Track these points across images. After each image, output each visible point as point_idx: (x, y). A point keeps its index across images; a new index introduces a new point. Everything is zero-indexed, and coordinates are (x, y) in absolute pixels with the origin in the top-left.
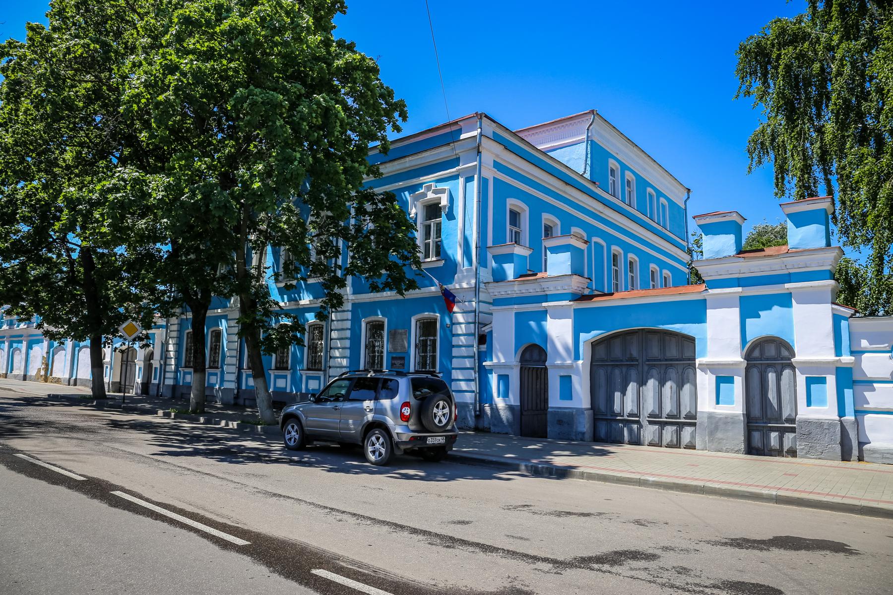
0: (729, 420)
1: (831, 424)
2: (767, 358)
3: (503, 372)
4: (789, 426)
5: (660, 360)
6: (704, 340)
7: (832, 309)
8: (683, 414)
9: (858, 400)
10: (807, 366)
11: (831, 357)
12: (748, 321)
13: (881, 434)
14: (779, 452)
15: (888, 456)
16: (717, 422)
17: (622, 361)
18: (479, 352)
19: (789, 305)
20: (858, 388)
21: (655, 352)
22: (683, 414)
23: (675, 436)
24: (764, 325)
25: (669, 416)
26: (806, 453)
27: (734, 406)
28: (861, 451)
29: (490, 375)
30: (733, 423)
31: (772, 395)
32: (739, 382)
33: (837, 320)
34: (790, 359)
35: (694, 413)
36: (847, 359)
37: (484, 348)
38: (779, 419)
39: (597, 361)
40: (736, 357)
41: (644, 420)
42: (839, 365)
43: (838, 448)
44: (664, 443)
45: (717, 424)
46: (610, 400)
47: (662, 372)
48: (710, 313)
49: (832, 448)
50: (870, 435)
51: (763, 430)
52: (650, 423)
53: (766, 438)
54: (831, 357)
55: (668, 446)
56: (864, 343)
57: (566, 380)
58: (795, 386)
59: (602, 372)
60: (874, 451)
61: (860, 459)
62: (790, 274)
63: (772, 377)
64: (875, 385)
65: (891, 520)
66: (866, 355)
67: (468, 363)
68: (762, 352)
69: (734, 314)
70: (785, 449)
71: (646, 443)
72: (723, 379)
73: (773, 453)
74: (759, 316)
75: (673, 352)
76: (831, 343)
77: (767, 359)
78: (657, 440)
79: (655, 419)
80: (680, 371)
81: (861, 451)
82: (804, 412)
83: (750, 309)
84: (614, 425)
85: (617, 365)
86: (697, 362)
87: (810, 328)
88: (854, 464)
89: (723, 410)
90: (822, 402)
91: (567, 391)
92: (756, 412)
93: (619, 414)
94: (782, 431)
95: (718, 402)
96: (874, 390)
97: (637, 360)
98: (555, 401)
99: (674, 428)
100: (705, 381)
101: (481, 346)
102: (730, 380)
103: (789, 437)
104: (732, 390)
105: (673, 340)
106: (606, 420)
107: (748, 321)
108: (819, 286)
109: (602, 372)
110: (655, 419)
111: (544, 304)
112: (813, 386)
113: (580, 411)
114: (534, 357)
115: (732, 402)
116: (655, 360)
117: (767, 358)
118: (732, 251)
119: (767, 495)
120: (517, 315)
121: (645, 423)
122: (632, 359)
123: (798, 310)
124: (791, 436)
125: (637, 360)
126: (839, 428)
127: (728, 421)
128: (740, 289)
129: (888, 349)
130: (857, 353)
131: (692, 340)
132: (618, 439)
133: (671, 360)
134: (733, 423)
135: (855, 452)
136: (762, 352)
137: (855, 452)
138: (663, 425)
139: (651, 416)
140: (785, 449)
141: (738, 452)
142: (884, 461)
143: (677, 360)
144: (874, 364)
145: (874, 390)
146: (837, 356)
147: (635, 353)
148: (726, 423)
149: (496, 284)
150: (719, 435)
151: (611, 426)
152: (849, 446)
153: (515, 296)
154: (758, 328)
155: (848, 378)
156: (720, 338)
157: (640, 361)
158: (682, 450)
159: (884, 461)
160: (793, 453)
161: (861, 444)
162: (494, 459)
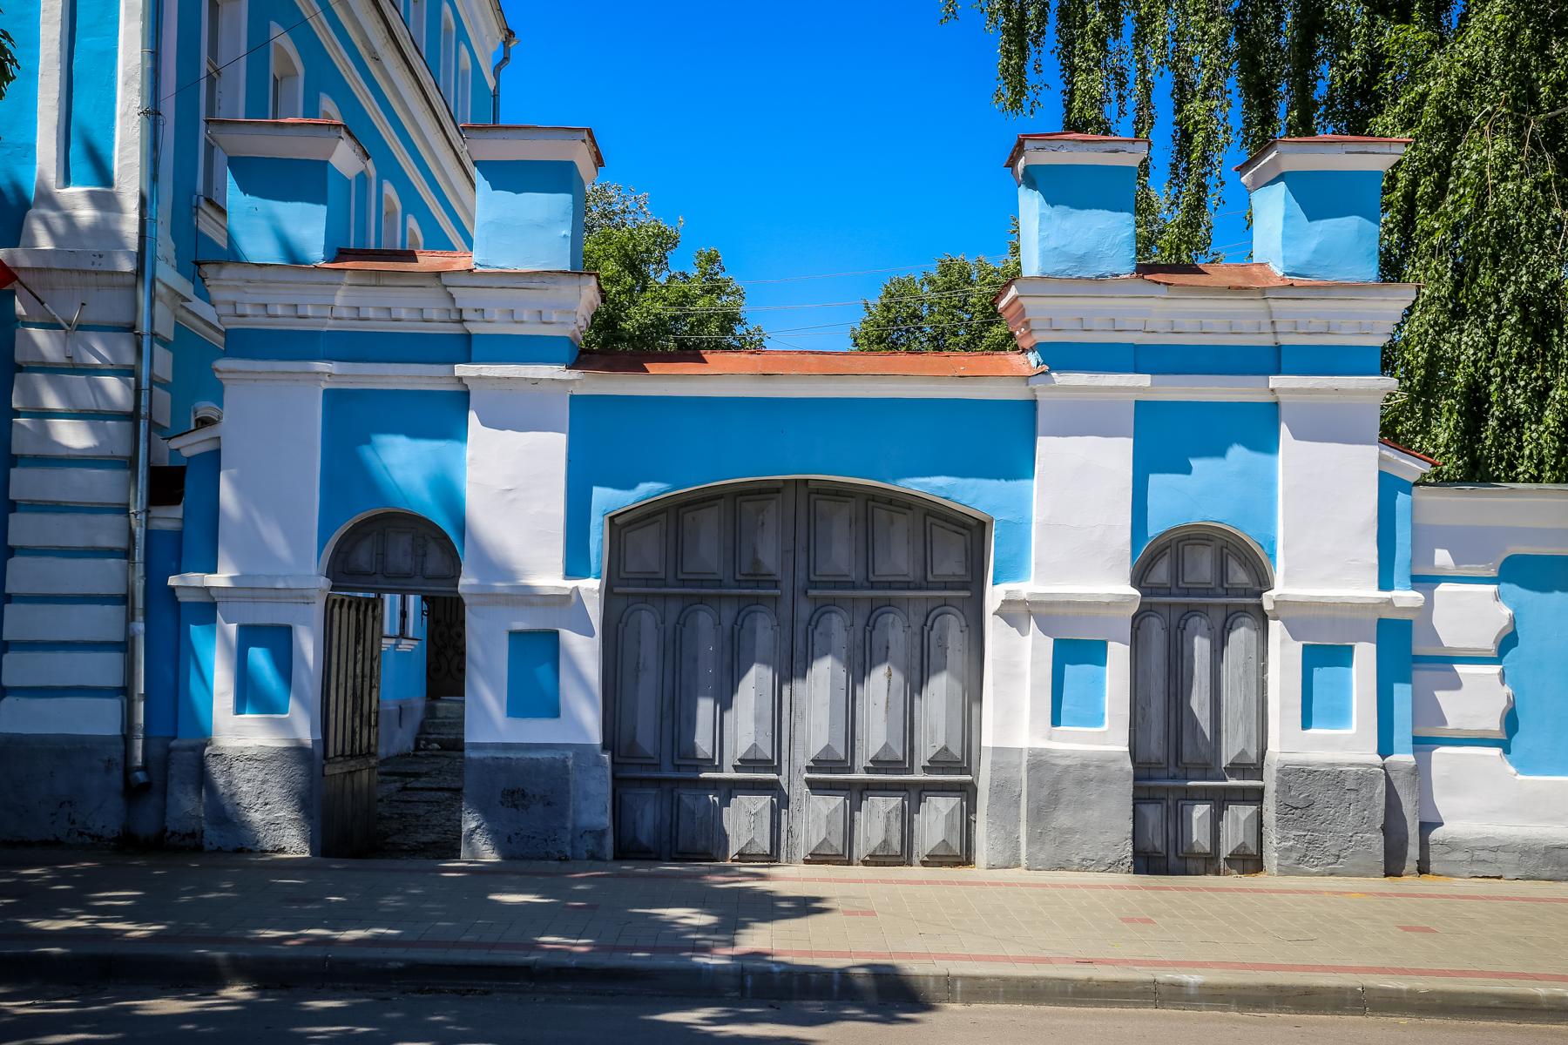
0: (1092, 772)
1: (1364, 778)
2: (1197, 587)
3: (265, 615)
4: (1242, 786)
5: (853, 586)
6: (1019, 529)
7: (1381, 458)
8: (922, 759)
9: (1426, 710)
10: (1300, 617)
11: (1369, 591)
12: (1155, 480)
13: (1478, 797)
14: (1208, 863)
15: (1484, 855)
16: (1058, 780)
17: (719, 583)
18: (149, 534)
19: (1265, 443)
20: (1422, 675)
21: (840, 556)
22: (922, 759)
23: (896, 826)
24: (1195, 494)
25: (878, 765)
26: (1299, 861)
27: (1105, 737)
28: (1424, 845)
29: (196, 631)
30: (1103, 781)
31: (1199, 702)
32: (1119, 655)
33: (1389, 486)
34: (1259, 595)
35: (956, 751)
36: (1405, 597)
37: (169, 517)
38: (1208, 767)
39: (628, 581)
40: (1115, 585)
41: (795, 781)
42: (1388, 615)
43: (1377, 842)
44: (861, 850)
45: (1051, 783)
46: (678, 721)
47: (860, 622)
48: (1046, 446)
49: (1362, 842)
50: (1443, 803)
51: (1179, 801)
52: (815, 787)
53: (1178, 821)
54: (1369, 591)
55: (874, 860)
56: (1442, 558)
57: (537, 650)
58: (1263, 669)
59: (647, 621)
60: (1451, 846)
61: (1423, 868)
62: (1278, 349)
63: (1201, 646)
64: (1459, 668)
65: (1563, 1027)
66: (1443, 588)
67: (105, 576)
68: (1177, 570)
69: (1117, 454)
70: (1225, 851)
71: (802, 853)
72: (1075, 654)
73: (1191, 864)
74: (1187, 470)
75: (898, 559)
76: (1370, 552)
77: (1188, 592)
78: (837, 843)
79: (831, 776)
80: (917, 621)
81: (1424, 845)
82: (1289, 743)
83: (1164, 441)
84: (687, 798)
85: (702, 599)
86: (994, 595)
87: (1319, 507)
88: (1409, 882)
89: (1073, 742)
90: (1339, 716)
91: (535, 692)
92: (1155, 748)
93: (709, 764)
94: (1221, 800)
95: (1056, 720)
96: (1456, 684)
97: (776, 584)
98: (490, 717)
99: (895, 802)
100: (1016, 660)
101: (158, 511)
102: (1093, 652)
103: (1238, 816)
104: (1098, 683)
105: (902, 523)
106: (658, 782)
107: (1155, 480)
108: (1357, 392)
109: (647, 621)
110: (831, 776)
111: (461, 370)
112: (1318, 673)
113: (582, 750)
114: (399, 557)
115: (1097, 720)
116: (837, 585)
117: (1197, 587)
118: (1122, 260)
119: (1550, 999)
120: (336, 400)
121: (798, 789)
122: (759, 578)
123: (1294, 459)
124: (1244, 812)
125: (776, 584)
126: (1381, 787)
127: (1087, 774)
128: (1144, 380)
129: (1493, 573)
130: (1425, 581)
131: (974, 531)
132: (701, 845)
133: (889, 585)
134: (1103, 781)
135: (1413, 851)
136: (1177, 570)
137: (1413, 851)
138: (858, 792)
139: (818, 765)
140: (1225, 851)
141: (1112, 867)
142: (1476, 869)
143: (908, 586)
144: (1467, 613)
145: (1456, 684)
146: (1381, 588)
147: (770, 557)
148: (1082, 782)
149: (1141, 285)
150: (1062, 819)
151: (676, 803)
152: (1404, 842)
153: (331, 325)
154: (1181, 499)
155: (1406, 653)
156: (1071, 524)
157: (786, 584)
158: (917, 872)
159: (1476, 869)
160: (1249, 861)
161: (1426, 827)
162: (477, 956)
